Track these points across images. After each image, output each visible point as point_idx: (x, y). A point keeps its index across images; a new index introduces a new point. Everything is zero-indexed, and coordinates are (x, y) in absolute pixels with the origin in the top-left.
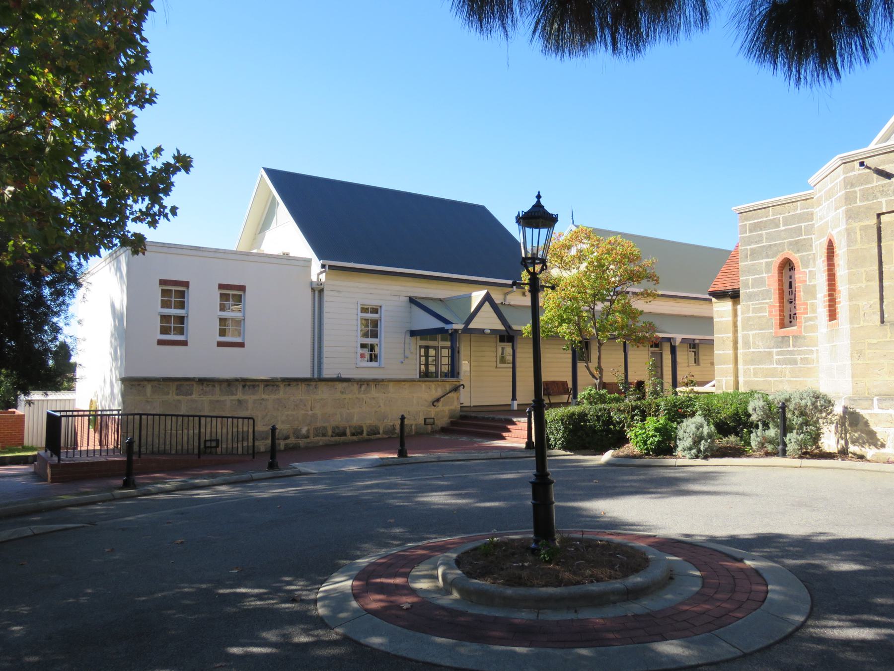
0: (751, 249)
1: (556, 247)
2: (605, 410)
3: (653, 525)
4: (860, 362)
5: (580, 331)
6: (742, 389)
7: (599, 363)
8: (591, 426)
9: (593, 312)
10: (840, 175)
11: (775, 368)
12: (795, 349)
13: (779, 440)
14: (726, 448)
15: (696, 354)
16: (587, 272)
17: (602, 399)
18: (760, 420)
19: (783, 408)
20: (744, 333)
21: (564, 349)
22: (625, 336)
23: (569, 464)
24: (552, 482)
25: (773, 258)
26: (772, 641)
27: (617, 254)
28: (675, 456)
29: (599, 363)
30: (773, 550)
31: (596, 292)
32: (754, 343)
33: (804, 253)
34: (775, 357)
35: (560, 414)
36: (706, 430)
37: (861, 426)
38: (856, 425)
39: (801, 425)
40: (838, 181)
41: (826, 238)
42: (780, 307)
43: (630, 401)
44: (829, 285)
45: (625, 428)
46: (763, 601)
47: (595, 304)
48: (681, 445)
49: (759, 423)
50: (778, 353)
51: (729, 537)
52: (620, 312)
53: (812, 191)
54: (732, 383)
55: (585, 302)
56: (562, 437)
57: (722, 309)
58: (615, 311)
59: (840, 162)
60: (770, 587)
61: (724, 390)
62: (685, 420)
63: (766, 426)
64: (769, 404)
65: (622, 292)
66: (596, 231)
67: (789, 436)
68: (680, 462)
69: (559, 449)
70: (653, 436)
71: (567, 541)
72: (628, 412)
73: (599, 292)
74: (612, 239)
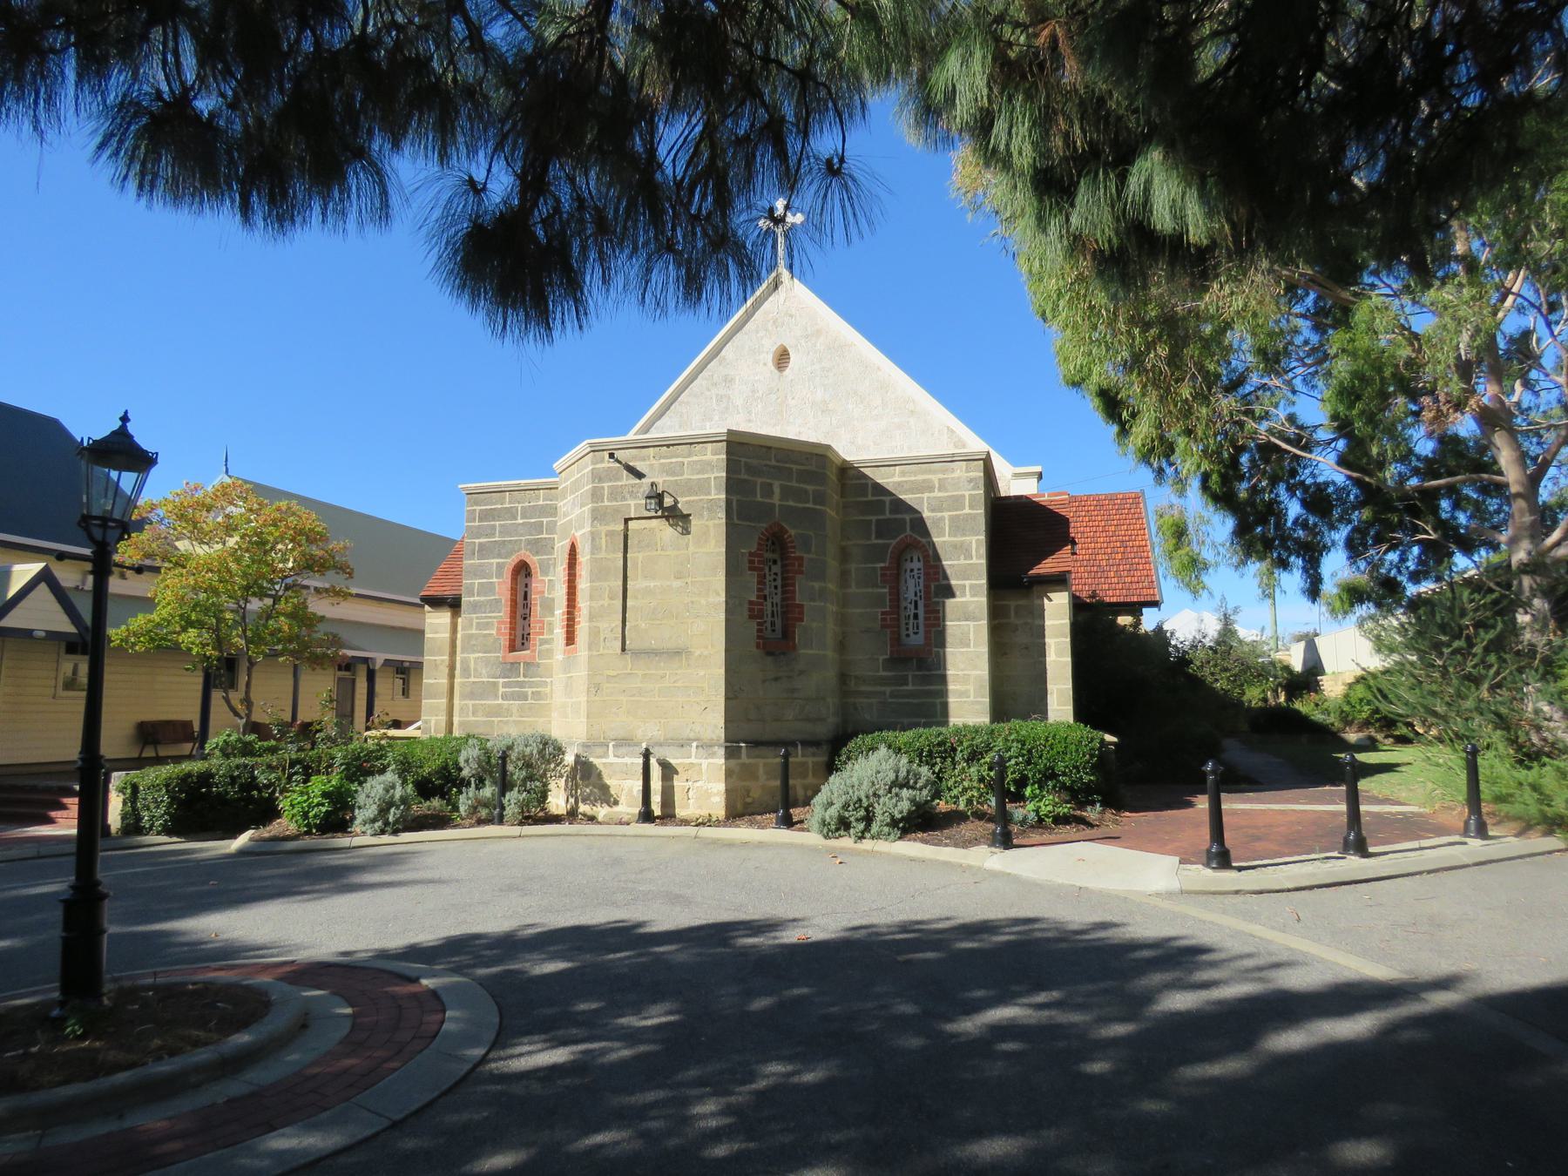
0: (480, 544)
1: (186, 504)
2: (246, 766)
3: (294, 945)
4: (597, 698)
5: (219, 643)
6: (456, 733)
7: (247, 693)
8: (219, 794)
9: (244, 613)
10: (587, 467)
11: (499, 705)
12: (526, 680)
13: (496, 802)
14: (426, 816)
15: (406, 682)
16: (236, 550)
17: (247, 750)
18: (473, 776)
19: (504, 757)
20: (465, 655)
21: (187, 669)
22: (293, 653)
23: (173, 858)
24: (103, 897)
25: (506, 558)
26: (436, 1094)
27: (287, 527)
28: (351, 832)
29: (247, 693)
30: (463, 958)
31: (251, 582)
32: (475, 670)
33: (545, 557)
34: (501, 690)
35: (164, 776)
36: (398, 793)
37: (593, 779)
38: (589, 778)
39: (524, 781)
40: (586, 471)
41: (568, 540)
42: (511, 623)
43: (290, 751)
44: (569, 600)
45: (277, 795)
46: (435, 1037)
47: (247, 601)
48: (360, 816)
49: (473, 779)
50: (505, 685)
51: (406, 947)
52: (287, 615)
53: (557, 479)
54: (444, 724)
55: (230, 597)
56: (165, 813)
57: (437, 622)
58: (279, 614)
59: (589, 449)
60: (448, 1014)
61: (433, 734)
62: (369, 779)
63: (481, 783)
64: (487, 754)
65: (294, 585)
66: (260, 490)
67: (508, 795)
68: (357, 841)
69: (159, 833)
70: (319, 805)
71: (132, 993)
72: (284, 770)
73: (256, 582)
74: (283, 504)
